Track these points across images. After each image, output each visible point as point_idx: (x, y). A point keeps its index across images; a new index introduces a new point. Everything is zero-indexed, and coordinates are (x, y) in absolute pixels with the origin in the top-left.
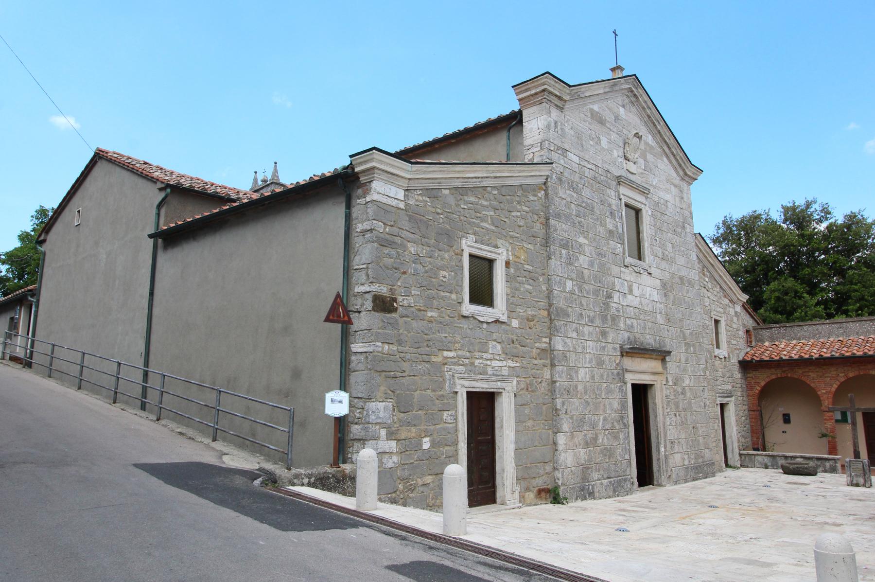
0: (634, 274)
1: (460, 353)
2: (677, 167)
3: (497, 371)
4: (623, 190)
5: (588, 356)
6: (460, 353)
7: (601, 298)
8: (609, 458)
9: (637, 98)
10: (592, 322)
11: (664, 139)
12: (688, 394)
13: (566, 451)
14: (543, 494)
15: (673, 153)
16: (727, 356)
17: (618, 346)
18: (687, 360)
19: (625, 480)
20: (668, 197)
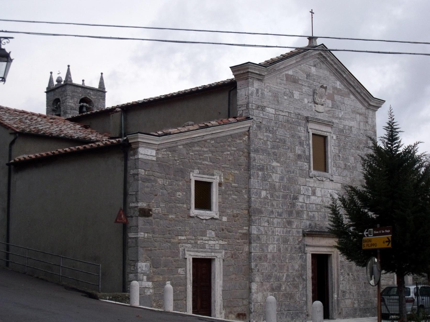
0: (318, 182)
2: (362, 100)
3: (213, 247)
7: (288, 201)
8: (290, 299)
9: (326, 58)
13: (257, 293)
14: (241, 316)
15: (357, 92)
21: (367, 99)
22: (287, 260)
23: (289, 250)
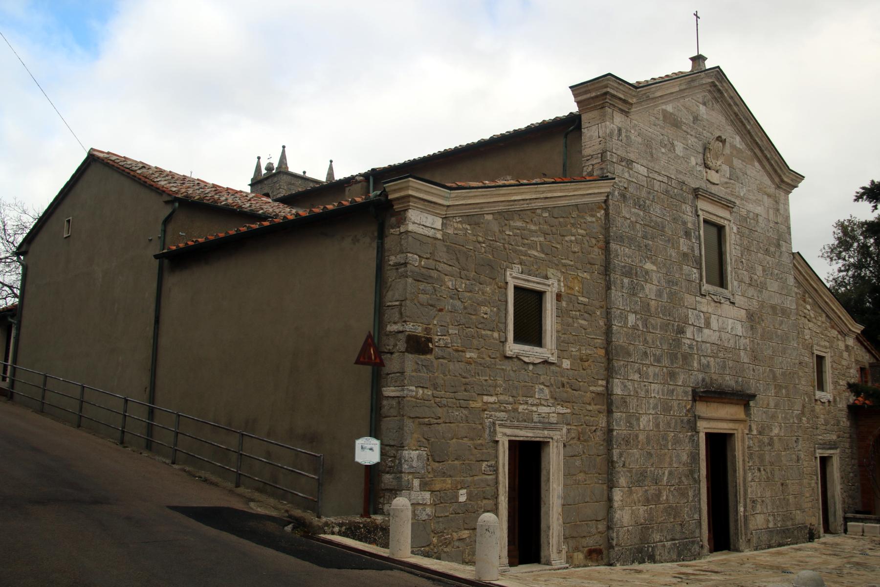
0: (713, 304)
1: (502, 398)
4: (702, 204)
5: (651, 401)
6: (502, 398)
8: (674, 518)
10: (659, 361)
11: (755, 141)
12: (777, 445)
15: (766, 157)
16: (831, 399)
17: (690, 389)
18: (777, 406)
19: (693, 542)
20: (759, 210)
21: (779, 171)
22: (670, 444)
23: (673, 425)
